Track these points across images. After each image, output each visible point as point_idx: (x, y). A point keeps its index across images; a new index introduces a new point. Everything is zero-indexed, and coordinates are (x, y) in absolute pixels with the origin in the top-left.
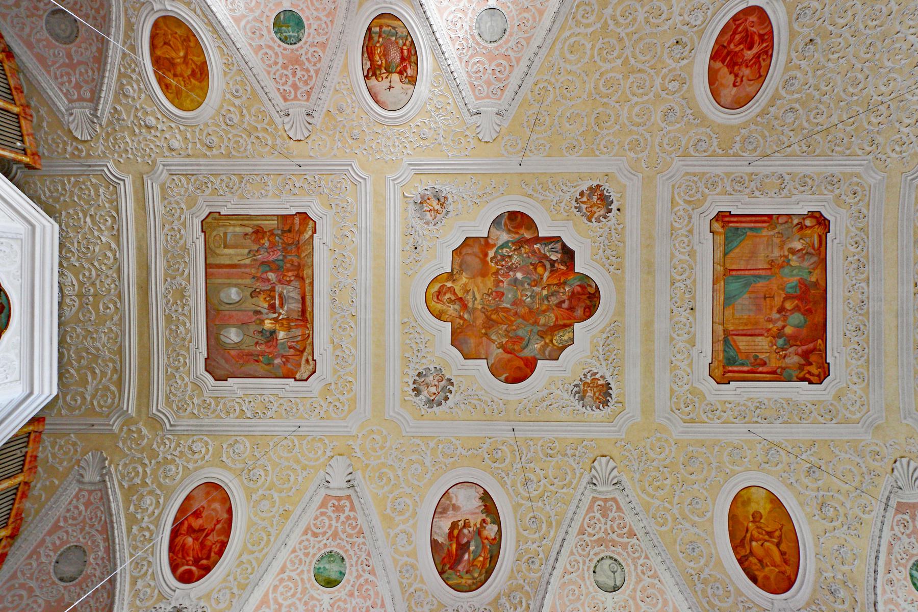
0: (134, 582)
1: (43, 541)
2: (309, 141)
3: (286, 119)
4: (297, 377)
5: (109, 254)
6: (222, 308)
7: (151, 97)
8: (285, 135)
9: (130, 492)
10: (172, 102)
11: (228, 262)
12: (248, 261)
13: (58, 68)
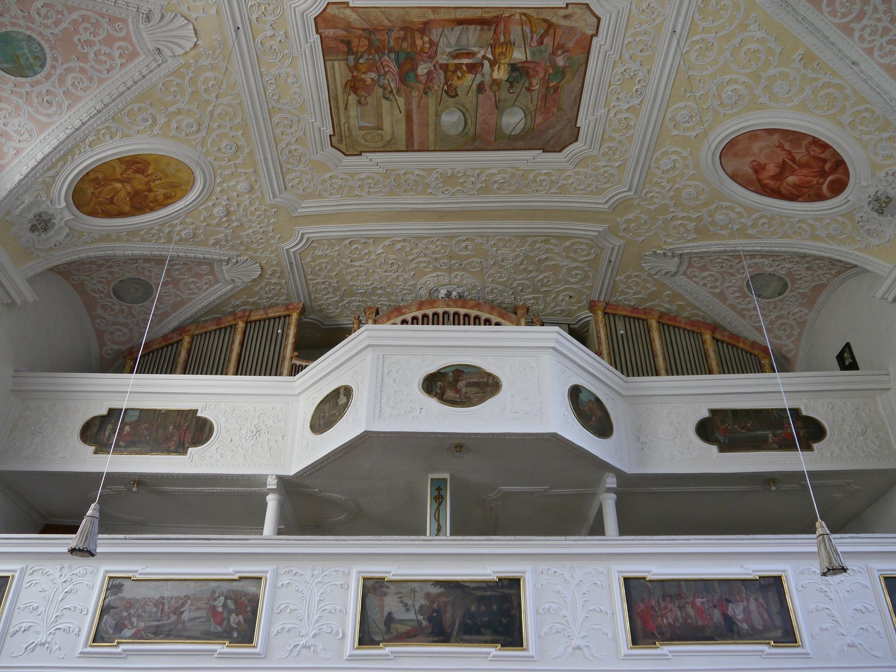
0: (817, 238)
1: (730, 306)
2: (193, 15)
3: (167, 52)
4: (590, 32)
5: (398, 246)
6: (471, 132)
7: (189, 212)
8: (193, 53)
9: (702, 232)
10: (185, 193)
11: (403, 126)
12: (401, 101)
13: (183, 293)
